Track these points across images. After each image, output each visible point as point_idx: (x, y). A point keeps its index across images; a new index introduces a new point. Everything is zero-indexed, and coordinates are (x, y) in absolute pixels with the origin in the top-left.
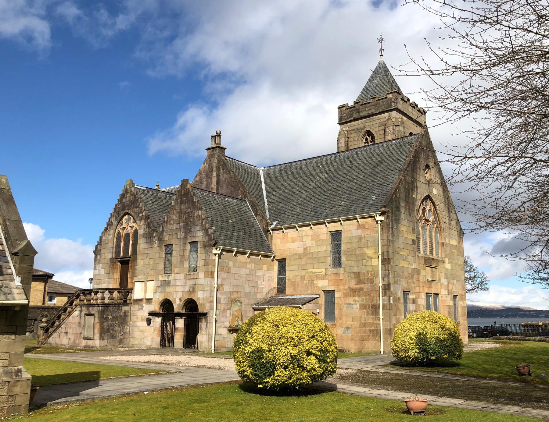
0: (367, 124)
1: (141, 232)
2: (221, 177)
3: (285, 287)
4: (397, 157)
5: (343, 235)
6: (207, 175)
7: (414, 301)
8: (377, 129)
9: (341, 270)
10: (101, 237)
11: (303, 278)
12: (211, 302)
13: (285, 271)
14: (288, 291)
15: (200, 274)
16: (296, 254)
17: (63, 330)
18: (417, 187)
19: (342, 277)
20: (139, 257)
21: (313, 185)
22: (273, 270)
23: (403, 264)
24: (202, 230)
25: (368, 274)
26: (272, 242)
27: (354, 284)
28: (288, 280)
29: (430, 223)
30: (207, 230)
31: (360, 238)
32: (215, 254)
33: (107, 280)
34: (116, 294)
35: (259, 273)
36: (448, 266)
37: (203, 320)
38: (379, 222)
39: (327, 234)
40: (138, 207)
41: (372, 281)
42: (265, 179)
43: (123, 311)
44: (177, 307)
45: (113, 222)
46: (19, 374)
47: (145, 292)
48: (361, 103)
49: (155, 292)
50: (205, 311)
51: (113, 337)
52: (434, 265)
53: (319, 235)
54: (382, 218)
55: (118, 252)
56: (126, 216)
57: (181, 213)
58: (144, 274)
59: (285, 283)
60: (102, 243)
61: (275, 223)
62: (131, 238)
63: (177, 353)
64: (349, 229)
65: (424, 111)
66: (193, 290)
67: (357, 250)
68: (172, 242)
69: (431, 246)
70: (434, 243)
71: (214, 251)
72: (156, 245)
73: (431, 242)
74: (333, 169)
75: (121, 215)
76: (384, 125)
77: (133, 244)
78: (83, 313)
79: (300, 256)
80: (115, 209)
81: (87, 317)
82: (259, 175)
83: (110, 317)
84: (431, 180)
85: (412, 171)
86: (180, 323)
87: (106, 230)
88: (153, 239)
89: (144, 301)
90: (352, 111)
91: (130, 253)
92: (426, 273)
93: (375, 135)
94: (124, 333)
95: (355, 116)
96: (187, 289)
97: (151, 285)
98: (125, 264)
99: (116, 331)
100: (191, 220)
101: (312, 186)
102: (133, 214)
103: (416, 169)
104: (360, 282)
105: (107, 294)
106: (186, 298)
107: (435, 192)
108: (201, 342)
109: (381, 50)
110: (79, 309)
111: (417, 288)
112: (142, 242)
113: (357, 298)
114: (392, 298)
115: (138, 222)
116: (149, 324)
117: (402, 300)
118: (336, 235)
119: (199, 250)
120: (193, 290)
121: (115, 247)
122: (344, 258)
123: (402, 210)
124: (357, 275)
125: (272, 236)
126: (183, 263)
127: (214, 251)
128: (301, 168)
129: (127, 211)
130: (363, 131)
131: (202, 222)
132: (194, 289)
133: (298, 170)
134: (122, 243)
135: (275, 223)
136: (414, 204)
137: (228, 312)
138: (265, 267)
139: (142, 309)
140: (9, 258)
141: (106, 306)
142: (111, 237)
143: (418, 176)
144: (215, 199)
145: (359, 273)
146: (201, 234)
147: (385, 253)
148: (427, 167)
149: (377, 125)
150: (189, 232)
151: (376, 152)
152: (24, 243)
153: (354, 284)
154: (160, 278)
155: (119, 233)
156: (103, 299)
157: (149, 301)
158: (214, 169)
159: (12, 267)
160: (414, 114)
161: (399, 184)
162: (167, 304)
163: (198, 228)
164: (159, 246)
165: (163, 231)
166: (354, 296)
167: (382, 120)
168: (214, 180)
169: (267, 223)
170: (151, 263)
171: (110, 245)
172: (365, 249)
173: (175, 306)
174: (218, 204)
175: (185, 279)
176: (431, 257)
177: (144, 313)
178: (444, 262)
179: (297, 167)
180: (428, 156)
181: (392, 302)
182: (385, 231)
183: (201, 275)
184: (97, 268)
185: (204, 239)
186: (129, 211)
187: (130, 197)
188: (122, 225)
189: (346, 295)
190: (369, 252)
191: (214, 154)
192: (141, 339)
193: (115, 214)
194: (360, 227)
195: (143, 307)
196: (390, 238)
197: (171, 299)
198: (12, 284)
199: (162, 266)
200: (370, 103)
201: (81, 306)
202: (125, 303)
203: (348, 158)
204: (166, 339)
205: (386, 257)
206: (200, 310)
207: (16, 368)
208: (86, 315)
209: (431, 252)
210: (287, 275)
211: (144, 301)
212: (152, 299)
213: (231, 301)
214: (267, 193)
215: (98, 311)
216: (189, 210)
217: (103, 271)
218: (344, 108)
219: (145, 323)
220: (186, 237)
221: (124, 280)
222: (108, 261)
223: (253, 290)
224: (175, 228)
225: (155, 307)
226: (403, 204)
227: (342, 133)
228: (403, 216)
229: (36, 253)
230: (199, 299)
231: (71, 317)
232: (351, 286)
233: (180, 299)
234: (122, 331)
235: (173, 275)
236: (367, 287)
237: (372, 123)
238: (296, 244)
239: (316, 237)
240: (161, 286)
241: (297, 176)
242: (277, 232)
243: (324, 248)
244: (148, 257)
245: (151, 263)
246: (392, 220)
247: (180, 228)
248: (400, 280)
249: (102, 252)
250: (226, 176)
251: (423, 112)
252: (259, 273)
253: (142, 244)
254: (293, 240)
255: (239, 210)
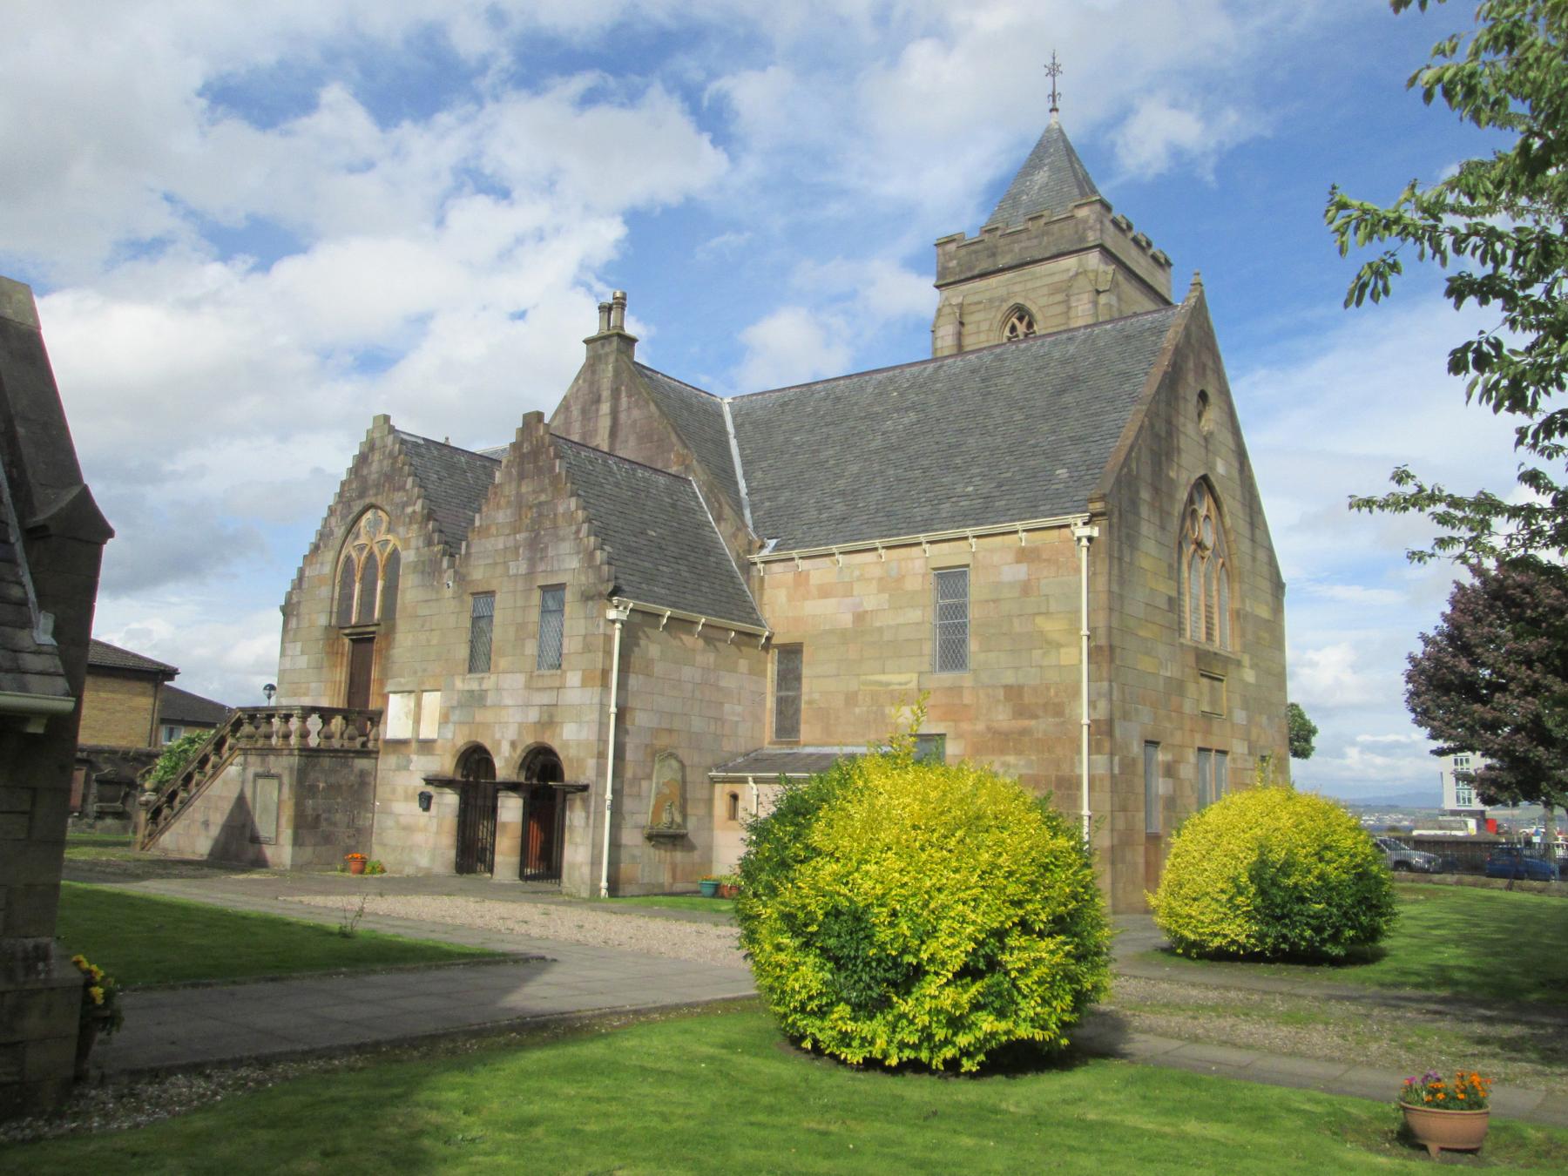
0: (1017, 288)
1: (408, 556)
2: (623, 417)
3: (798, 723)
4: (1123, 366)
5: (972, 577)
6: (584, 412)
7: (1170, 771)
8: (1043, 301)
9: (965, 679)
10: (301, 571)
11: (851, 699)
12: (602, 755)
13: (798, 678)
14: (808, 731)
15: (569, 675)
16: (832, 632)
17: (199, 817)
18: (1179, 450)
19: (968, 699)
20: (402, 625)
21: (877, 443)
22: (763, 674)
23: (1146, 664)
24: (578, 553)
25: (1048, 689)
26: (762, 595)
27: (1002, 718)
28: (810, 702)
29: (1208, 553)
30: (591, 555)
31: (1026, 588)
32: (614, 622)
33: (313, 685)
34: (337, 723)
35: (728, 681)
36: (1249, 676)
37: (578, 803)
38: (1084, 542)
39: (924, 576)
40: (402, 488)
41: (1058, 710)
42: (737, 427)
43: (356, 770)
44: (505, 765)
45: (336, 530)
46: (41, 966)
47: (417, 721)
48: (999, 233)
49: (445, 720)
50: (583, 781)
51: (328, 839)
52: (1217, 672)
53: (901, 579)
54: (1095, 532)
55: (345, 610)
56: (369, 515)
57: (520, 504)
58: (415, 673)
59: (798, 711)
60: (305, 585)
61: (773, 542)
62: (380, 574)
63: (501, 892)
64: (993, 557)
65: (1167, 261)
66: (549, 721)
67: (1016, 621)
68: (494, 585)
69: (1209, 619)
70: (1216, 610)
71: (612, 614)
72: (448, 593)
73: (1209, 607)
74: (932, 400)
75: (356, 509)
76: (1065, 290)
77: (385, 589)
78: (251, 771)
79: (844, 636)
80: (341, 495)
81: (260, 782)
82: (721, 416)
83: (321, 785)
84: (1211, 433)
85: (1169, 404)
86: (511, 809)
87: (316, 548)
88: (441, 576)
89: (414, 745)
90: (976, 252)
91: (377, 614)
92: (1197, 695)
93: (1038, 317)
94: (359, 830)
95: (985, 265)
96: (533, 715)
97: (433, 702)
98: (361, 647)
99: (335, 824)
100: (548, 524)
101: (873, 445)
102: (388, 508)
103: (1177, 398)
104: (1021, 711)
105: (314, 723)
106: (530, 740)
107: (1220, 468)
108: (572, 866)
109: (1054, 96)
110: (239, 759)
111: (1178, 734)
112: (410, 584)
113: (1011, 759)
114: (1116, 759)
115: (401, 530)
116: (427, 808)
117: (1140, 768)
118: (951, 580)
119: (567, 609)
120: (549, 721)
121: (336, 595)
122: (973, 645)
123: (1145, 511)
124: (1013, 693)
125: (762, 579)
126: (523, 646)
127: (612, 614)
128: (838, 399)
129: (373, 500)
130: (1005, 307)
131: (578, 532)
132: (551, 716)
133: (829, 402)
134: (357, 587)
135: (773, 542)
136: (1171, 497)
137: (644, 784)
138: (743, 665)
139: (406, 768)
140: (19, 548)
141: (309, 753)
142: (327, 569)
143: (1182, 419)
144: (611, 471)
145: (1020, 688)
146: (574, 563)
147: (1102, 632)
148: (1203, 396)
149: (1045, 291)
150: (542, 559)
151: (1057, 355)
152: (75, 491)
153: (1002, 718)
154: (459, 684)
155: (349, 559)
156: (304, 735)
157: (426, 746)
158: (606, 394)
159: (27, 579)
160: (1141, 265)
161: (1137, 438)
162: (475, 759)
163: (566, 547)
164: (458, 597)
165: (468, 554)
166: (1003, 752)
167: (1056, 279)
168: (605, 424)
169: (750, 543)
170: (434, 642)
171: (325, 591)
172: (1039, 620)
173: (499, 763)
174: (617, 485)
175: (528, 687)
176: (1207, 647)
177: (415, 781)
178: (1239, 664)
179: (828, 395)
180: (1204, 366)
181: (1116, 771)
182: (1102, 567)
183: (573, 678)
184: (289, 652)
185: (583, 578)
186: (379, 500)
187: (381, 461)
188: (357, 536)
189: (978, 749)
190: (1052, 627)
191: (607, 355)
192: (403, 848)
193: (339, 507)
194: (1024, 555)
195: (409, 761)
196: (1115, 588)
197: (488, 746)
198: (23, 638)
199: (463, 652)
200: (1026, 230)
201: (245, 752)
202: (365, 752)
203: (973, 372)
204: (472, 854)
205: (1103, 641)
206: (569, 777)
207: (30, 943)
208: (257, 776)
209: (1209, 635)
210: (805, 687)
211: (414, 745)
212: (433, 741)
213: (654, 755)
214: (746, 463)
215: (291, 769)
216: (543, 498)
217: (303, 662)
218: (952, 247)
219: (415, 806)
220: (531, 573)
221: (358, 685)
222: (318, 633)
223: (712, 727)
224: (501, 546)
225: (445, 764)
226: (1145, 495)
227: (947, 310)
228: (1146, 529)
229: (110, 533)
230: (566, 744)
231: (218, 782)
232: (995, 725)
233: (513, 744)
234: (351, 824)
235: (493, 678)
236: (1042, 726)
237: (1030, 285)
238: (833, 601)
239: (891, 584)
240: (461, 705)
241: (828, 419)
242: (776, 567)
243: (915, 615)
244: (426, 620)
245: (434, 642)
246: (1119, 539)
247: (517, 548)
248: (1136, 710)
249: (303, 609)
250: (636, 413)
251: (1163, 264)
252: (728, 681)
253: (410, 590)
254: (825, 592)
255: (674, 506)
